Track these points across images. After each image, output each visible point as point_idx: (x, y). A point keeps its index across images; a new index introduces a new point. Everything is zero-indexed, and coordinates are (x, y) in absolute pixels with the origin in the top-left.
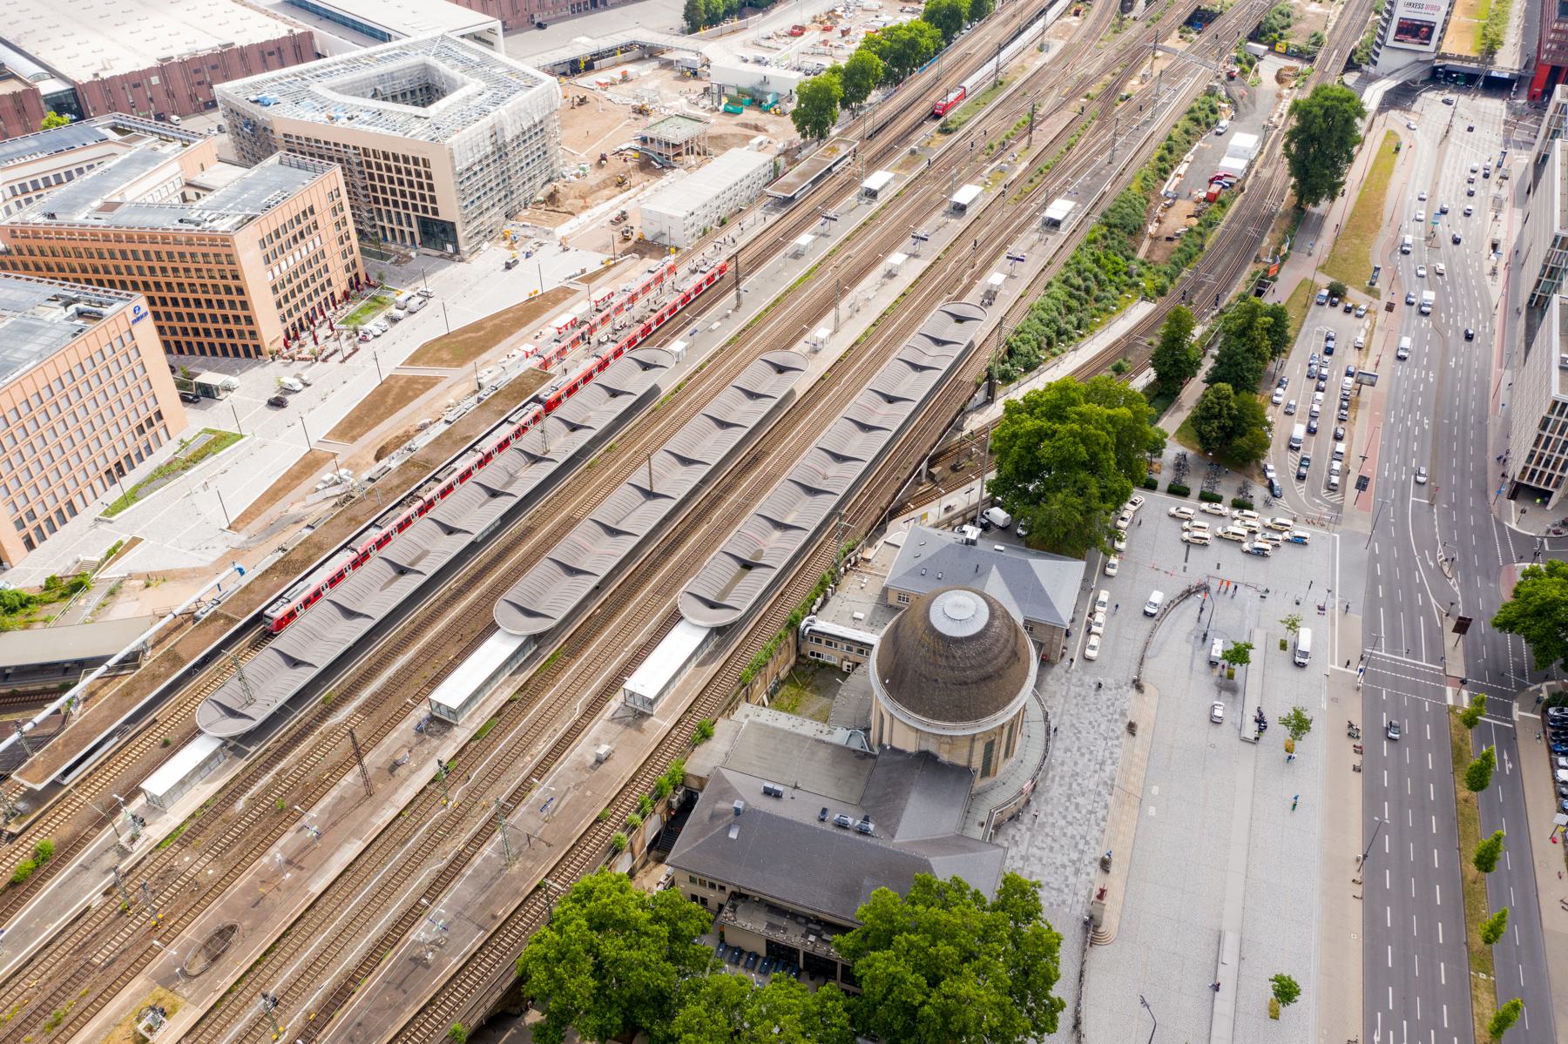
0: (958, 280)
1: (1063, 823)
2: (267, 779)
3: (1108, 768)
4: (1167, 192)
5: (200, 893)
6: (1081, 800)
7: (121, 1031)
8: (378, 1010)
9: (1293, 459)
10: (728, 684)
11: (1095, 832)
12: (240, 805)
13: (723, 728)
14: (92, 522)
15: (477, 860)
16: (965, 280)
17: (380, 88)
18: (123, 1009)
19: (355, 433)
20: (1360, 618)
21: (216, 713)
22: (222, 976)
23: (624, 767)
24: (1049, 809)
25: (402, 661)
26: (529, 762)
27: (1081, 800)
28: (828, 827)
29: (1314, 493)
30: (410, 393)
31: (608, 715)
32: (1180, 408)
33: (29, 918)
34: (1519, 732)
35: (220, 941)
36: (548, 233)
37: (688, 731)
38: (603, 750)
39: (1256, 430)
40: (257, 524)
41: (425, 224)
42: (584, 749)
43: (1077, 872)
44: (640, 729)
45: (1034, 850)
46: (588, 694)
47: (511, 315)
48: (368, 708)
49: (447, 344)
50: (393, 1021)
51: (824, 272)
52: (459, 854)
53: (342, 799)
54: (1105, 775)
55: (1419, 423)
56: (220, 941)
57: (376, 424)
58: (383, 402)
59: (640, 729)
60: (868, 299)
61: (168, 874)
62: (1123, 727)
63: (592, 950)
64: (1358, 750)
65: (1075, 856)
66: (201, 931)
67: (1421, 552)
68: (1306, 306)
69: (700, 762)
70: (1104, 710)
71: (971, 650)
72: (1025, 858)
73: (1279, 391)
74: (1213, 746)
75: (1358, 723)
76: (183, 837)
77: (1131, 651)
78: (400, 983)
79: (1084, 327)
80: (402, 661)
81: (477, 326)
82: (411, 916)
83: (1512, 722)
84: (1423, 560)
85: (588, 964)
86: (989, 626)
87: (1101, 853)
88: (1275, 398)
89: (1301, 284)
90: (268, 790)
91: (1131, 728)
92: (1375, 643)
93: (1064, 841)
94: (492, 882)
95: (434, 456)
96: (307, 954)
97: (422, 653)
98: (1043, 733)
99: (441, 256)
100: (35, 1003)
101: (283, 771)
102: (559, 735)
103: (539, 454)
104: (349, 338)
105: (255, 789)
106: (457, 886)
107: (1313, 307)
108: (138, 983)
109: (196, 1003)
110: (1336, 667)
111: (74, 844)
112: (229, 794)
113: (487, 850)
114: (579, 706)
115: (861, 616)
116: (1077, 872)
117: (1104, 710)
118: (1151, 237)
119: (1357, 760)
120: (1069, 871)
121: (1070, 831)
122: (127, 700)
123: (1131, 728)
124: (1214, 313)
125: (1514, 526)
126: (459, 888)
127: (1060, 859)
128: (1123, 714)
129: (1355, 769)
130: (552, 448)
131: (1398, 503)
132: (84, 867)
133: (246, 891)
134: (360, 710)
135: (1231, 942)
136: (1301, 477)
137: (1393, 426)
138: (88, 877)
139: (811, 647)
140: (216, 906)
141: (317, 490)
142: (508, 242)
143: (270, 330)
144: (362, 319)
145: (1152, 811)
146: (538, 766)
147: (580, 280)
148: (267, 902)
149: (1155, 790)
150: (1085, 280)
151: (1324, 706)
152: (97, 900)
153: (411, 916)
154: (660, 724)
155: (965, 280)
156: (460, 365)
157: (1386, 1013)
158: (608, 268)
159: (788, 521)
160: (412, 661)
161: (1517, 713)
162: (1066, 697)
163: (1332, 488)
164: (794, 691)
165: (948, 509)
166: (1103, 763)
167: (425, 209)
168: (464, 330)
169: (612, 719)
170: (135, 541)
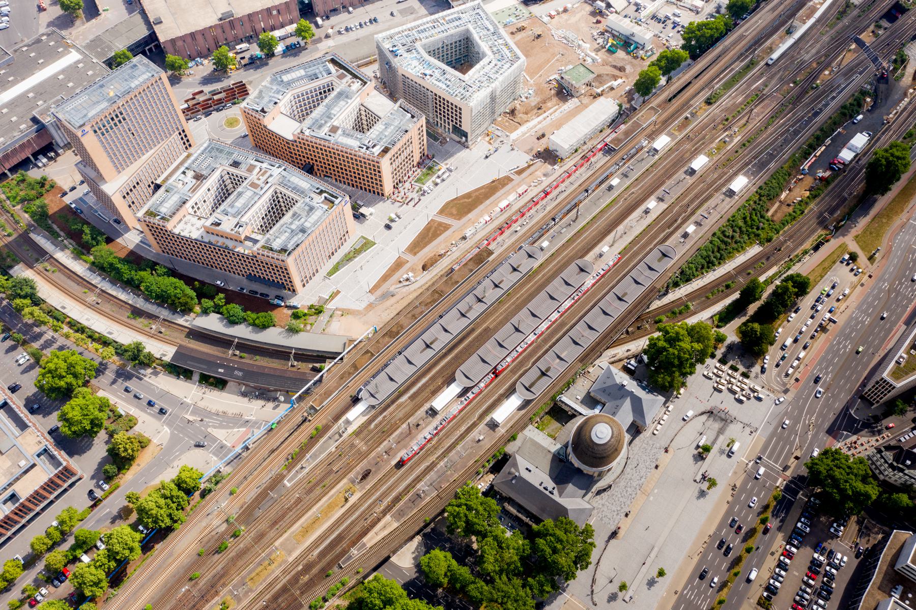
0: (676, 221)
1: (620, 496)
2: (380, 418)
3: (643, 480)
4: (803, 169)
5: (363, 456)
6: (629, 489)
7: (341, 494)
8: (407, 508)
9: (780, 354)
10: (526, 419)
11: (629, 502)
12: (372, 426)
13: (520, 437)
14: (323, 278)
15: (439, 466)
16: (679, 221)
17: (445, 41)
18: (341, 488)
19: (416, 250)
20: (765, 439)
21: (368, 395)
22: (367, 485)
23: (487, 444)
24: (617, 489)
25: (424, 380)
26: (458, 433)
27: (629, 489)
28: (541, 488)
29: (779, 375)
30: (438, 232)
31: (485, 422)
32: (745, 315)
33: (316, 451)
34: (795, 504)
35: (366, 475)
36: (507, 136)
37: (508, 436)
38: (481, 438)
39: (764, 346)
40: (379, 292)
41: (455, 128)
42: (475, 434)
43: (618, 514)
44: (494, 431)
45: (607, 503)
46: (481, 411)
47: (483, 190)
48: (412, 398)
49: (456, 204)
50: (411, 512)
51: (619, 201)
52: (433, 462)
53: (402, 433)
54: (641, 482)
55: (845, 347)
56: (366, 475)
57: (424, 247)
58: (428, 235)
59: (494, 431)
60: (631, 227)
61: (352, 446)
62: (654, 465)
63: (466, 516)
64: (732, 495)
65: (619, 509)
66: (362, 469)
67: (806, 416)
68: (834, 262)
69: (510, 448)
70: (651, 457)
71: (602, 448)
72: (603, 505)
73: (793, 315)
74: (683, 480)
75: (738, 486)
76: (357, 433)
77: (671, 434)
78: (413, 501)
79: (721, 260)
80: (424, 380)
81: (468, 195)
82: (418, 479)
83: (795, 499)
84: (805, 420)
85: (464, 519)
86: (610, 441)
87: (627, 511)
88: (790, 319)
89: (840, 247)
90: (380, 423)
91: (657, 467)
92: (764, 453)
93: (617, 502)
94: (442, 475)
95: (444, 289)
96: (389, 483)
97: (431, 379)
98: (621, 471)
99: (459, 142)
100: (318, 478)
101: (385, 416)
102: (469, 425)
103: (480, 297)
104: (418, 192)
105: (376, 421)
106: (432, 473)
107: (838, 263)
108: (345, 481)
109: (360, 491)
110: (743, 459)
111: (326, 428)
112: (370, 422)
113: (442, 463)
114: (477, 415)
115: (579, 398)
116: (618, 514)
117: (651, 457)
118: (780, 202)
119: (730, 499)
120: (616, 513)
121: (621, 499)
122: (342, 381)
123: (657, 467)
124: (786, 260)
125: (852, 412)
126: (432, 475)
127: (614, 508)
128: (657, 460)
129: (728, 502)
130: (486, 295)
131: (811, 389)
132: (330, 438)
133: (374, 458)
134: (409, 398)
135: (656, 549)
136: (777, 366)
137: (834, 346)
138: (331, 441)
139: (559, 403)
140: (365, 461)
141: (400, 282)
142: (487, 139)
143: (388, 187)
144: (423, 181)
145: (651, 498)
146: (461, 435)
147: (515, 172)
148: (379, 464)
149: (656, 491)
150: (734, 231)
151: (730, 475)
152: (334, 450)
153: (418, 479)
154: (501, 431)
155: (679, 221)
156: (459, 219)
157: (692, 585)
158: (529, 166)
159: (562, 356)
160: (427, 382)
161: (800, 495)
162: (640, 448)
163: (787, 375)
164: (549, 418)
165: (628, 350)
166: (642, 477)
167: (456, 123)
168: (464, 197)
169: (486, 425)
170: (338, 292)
